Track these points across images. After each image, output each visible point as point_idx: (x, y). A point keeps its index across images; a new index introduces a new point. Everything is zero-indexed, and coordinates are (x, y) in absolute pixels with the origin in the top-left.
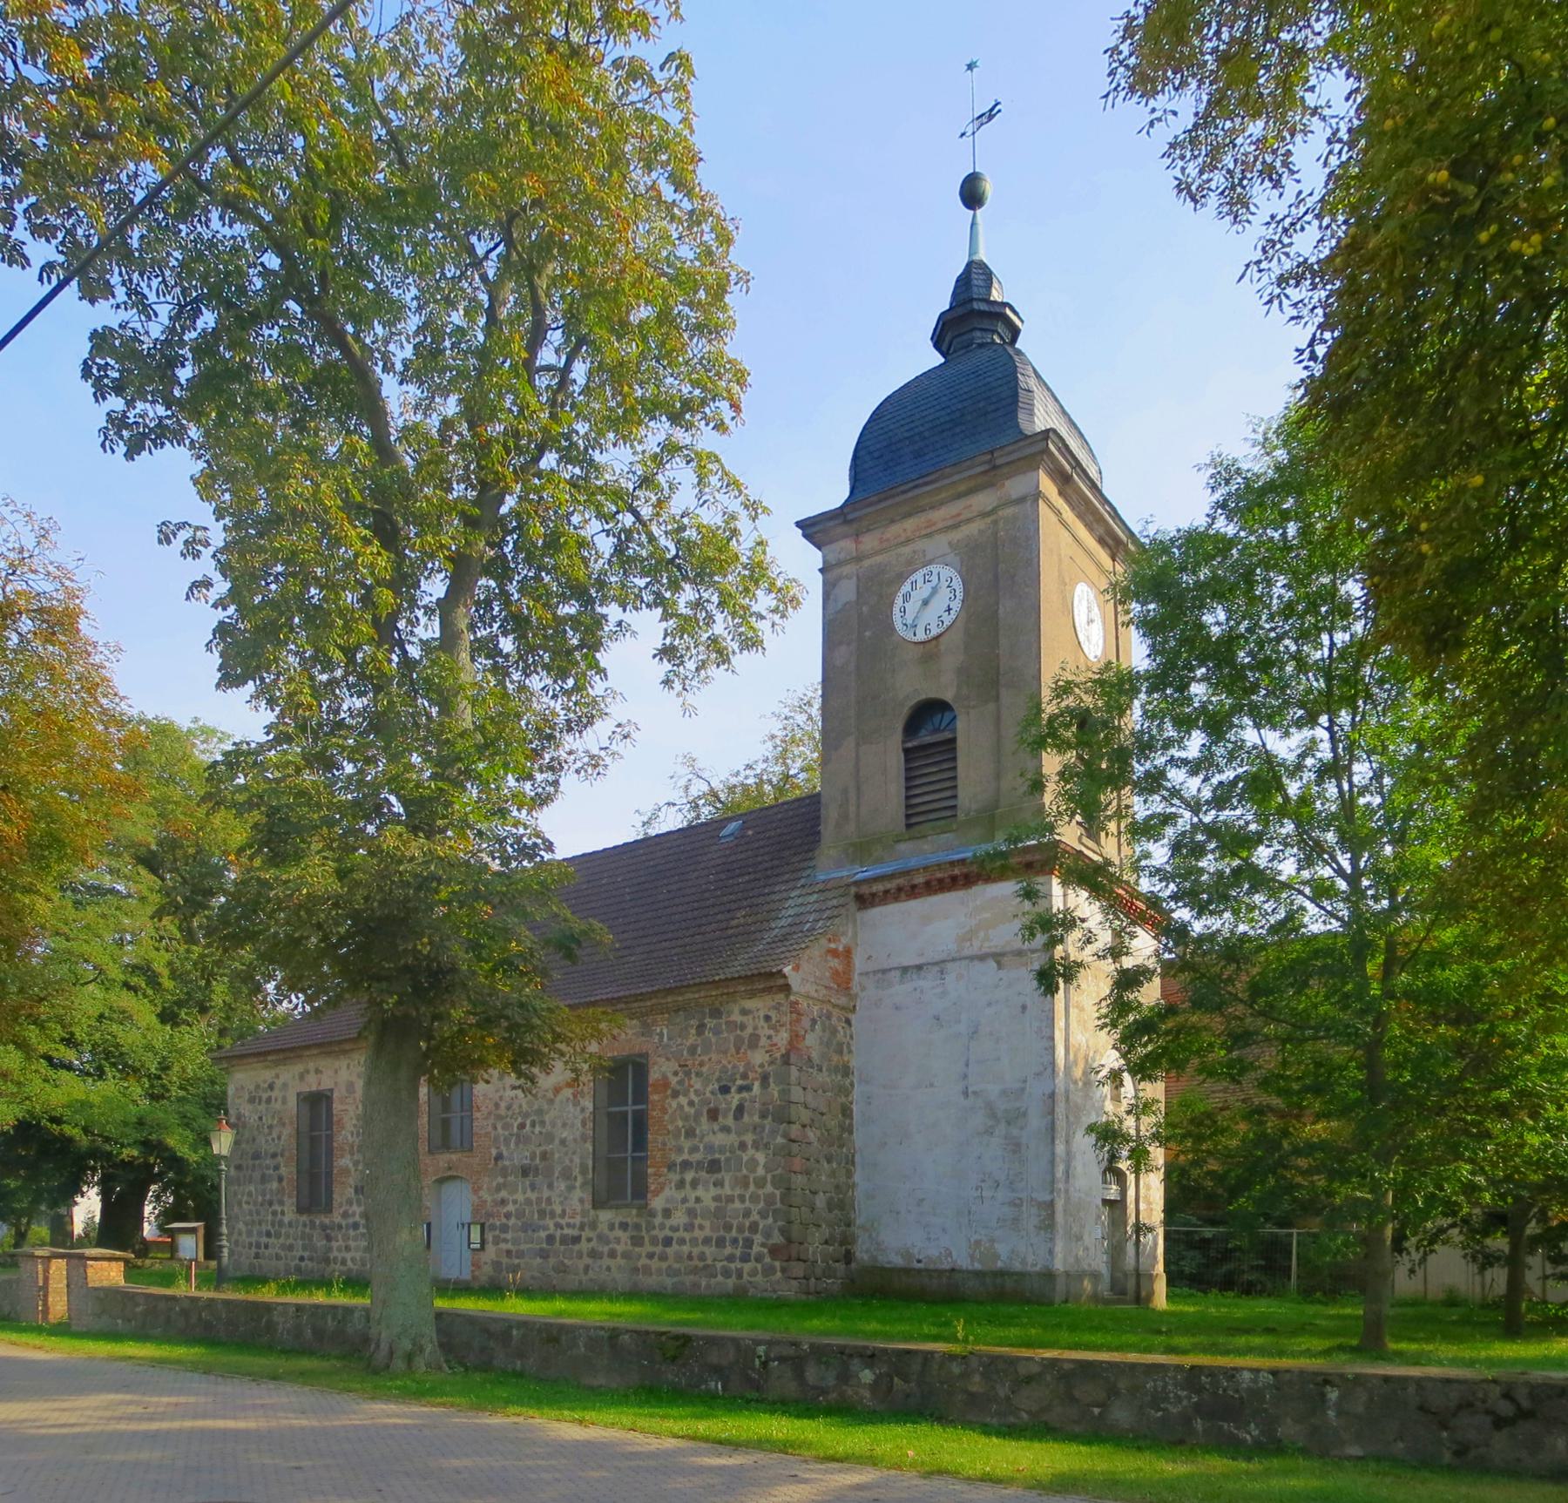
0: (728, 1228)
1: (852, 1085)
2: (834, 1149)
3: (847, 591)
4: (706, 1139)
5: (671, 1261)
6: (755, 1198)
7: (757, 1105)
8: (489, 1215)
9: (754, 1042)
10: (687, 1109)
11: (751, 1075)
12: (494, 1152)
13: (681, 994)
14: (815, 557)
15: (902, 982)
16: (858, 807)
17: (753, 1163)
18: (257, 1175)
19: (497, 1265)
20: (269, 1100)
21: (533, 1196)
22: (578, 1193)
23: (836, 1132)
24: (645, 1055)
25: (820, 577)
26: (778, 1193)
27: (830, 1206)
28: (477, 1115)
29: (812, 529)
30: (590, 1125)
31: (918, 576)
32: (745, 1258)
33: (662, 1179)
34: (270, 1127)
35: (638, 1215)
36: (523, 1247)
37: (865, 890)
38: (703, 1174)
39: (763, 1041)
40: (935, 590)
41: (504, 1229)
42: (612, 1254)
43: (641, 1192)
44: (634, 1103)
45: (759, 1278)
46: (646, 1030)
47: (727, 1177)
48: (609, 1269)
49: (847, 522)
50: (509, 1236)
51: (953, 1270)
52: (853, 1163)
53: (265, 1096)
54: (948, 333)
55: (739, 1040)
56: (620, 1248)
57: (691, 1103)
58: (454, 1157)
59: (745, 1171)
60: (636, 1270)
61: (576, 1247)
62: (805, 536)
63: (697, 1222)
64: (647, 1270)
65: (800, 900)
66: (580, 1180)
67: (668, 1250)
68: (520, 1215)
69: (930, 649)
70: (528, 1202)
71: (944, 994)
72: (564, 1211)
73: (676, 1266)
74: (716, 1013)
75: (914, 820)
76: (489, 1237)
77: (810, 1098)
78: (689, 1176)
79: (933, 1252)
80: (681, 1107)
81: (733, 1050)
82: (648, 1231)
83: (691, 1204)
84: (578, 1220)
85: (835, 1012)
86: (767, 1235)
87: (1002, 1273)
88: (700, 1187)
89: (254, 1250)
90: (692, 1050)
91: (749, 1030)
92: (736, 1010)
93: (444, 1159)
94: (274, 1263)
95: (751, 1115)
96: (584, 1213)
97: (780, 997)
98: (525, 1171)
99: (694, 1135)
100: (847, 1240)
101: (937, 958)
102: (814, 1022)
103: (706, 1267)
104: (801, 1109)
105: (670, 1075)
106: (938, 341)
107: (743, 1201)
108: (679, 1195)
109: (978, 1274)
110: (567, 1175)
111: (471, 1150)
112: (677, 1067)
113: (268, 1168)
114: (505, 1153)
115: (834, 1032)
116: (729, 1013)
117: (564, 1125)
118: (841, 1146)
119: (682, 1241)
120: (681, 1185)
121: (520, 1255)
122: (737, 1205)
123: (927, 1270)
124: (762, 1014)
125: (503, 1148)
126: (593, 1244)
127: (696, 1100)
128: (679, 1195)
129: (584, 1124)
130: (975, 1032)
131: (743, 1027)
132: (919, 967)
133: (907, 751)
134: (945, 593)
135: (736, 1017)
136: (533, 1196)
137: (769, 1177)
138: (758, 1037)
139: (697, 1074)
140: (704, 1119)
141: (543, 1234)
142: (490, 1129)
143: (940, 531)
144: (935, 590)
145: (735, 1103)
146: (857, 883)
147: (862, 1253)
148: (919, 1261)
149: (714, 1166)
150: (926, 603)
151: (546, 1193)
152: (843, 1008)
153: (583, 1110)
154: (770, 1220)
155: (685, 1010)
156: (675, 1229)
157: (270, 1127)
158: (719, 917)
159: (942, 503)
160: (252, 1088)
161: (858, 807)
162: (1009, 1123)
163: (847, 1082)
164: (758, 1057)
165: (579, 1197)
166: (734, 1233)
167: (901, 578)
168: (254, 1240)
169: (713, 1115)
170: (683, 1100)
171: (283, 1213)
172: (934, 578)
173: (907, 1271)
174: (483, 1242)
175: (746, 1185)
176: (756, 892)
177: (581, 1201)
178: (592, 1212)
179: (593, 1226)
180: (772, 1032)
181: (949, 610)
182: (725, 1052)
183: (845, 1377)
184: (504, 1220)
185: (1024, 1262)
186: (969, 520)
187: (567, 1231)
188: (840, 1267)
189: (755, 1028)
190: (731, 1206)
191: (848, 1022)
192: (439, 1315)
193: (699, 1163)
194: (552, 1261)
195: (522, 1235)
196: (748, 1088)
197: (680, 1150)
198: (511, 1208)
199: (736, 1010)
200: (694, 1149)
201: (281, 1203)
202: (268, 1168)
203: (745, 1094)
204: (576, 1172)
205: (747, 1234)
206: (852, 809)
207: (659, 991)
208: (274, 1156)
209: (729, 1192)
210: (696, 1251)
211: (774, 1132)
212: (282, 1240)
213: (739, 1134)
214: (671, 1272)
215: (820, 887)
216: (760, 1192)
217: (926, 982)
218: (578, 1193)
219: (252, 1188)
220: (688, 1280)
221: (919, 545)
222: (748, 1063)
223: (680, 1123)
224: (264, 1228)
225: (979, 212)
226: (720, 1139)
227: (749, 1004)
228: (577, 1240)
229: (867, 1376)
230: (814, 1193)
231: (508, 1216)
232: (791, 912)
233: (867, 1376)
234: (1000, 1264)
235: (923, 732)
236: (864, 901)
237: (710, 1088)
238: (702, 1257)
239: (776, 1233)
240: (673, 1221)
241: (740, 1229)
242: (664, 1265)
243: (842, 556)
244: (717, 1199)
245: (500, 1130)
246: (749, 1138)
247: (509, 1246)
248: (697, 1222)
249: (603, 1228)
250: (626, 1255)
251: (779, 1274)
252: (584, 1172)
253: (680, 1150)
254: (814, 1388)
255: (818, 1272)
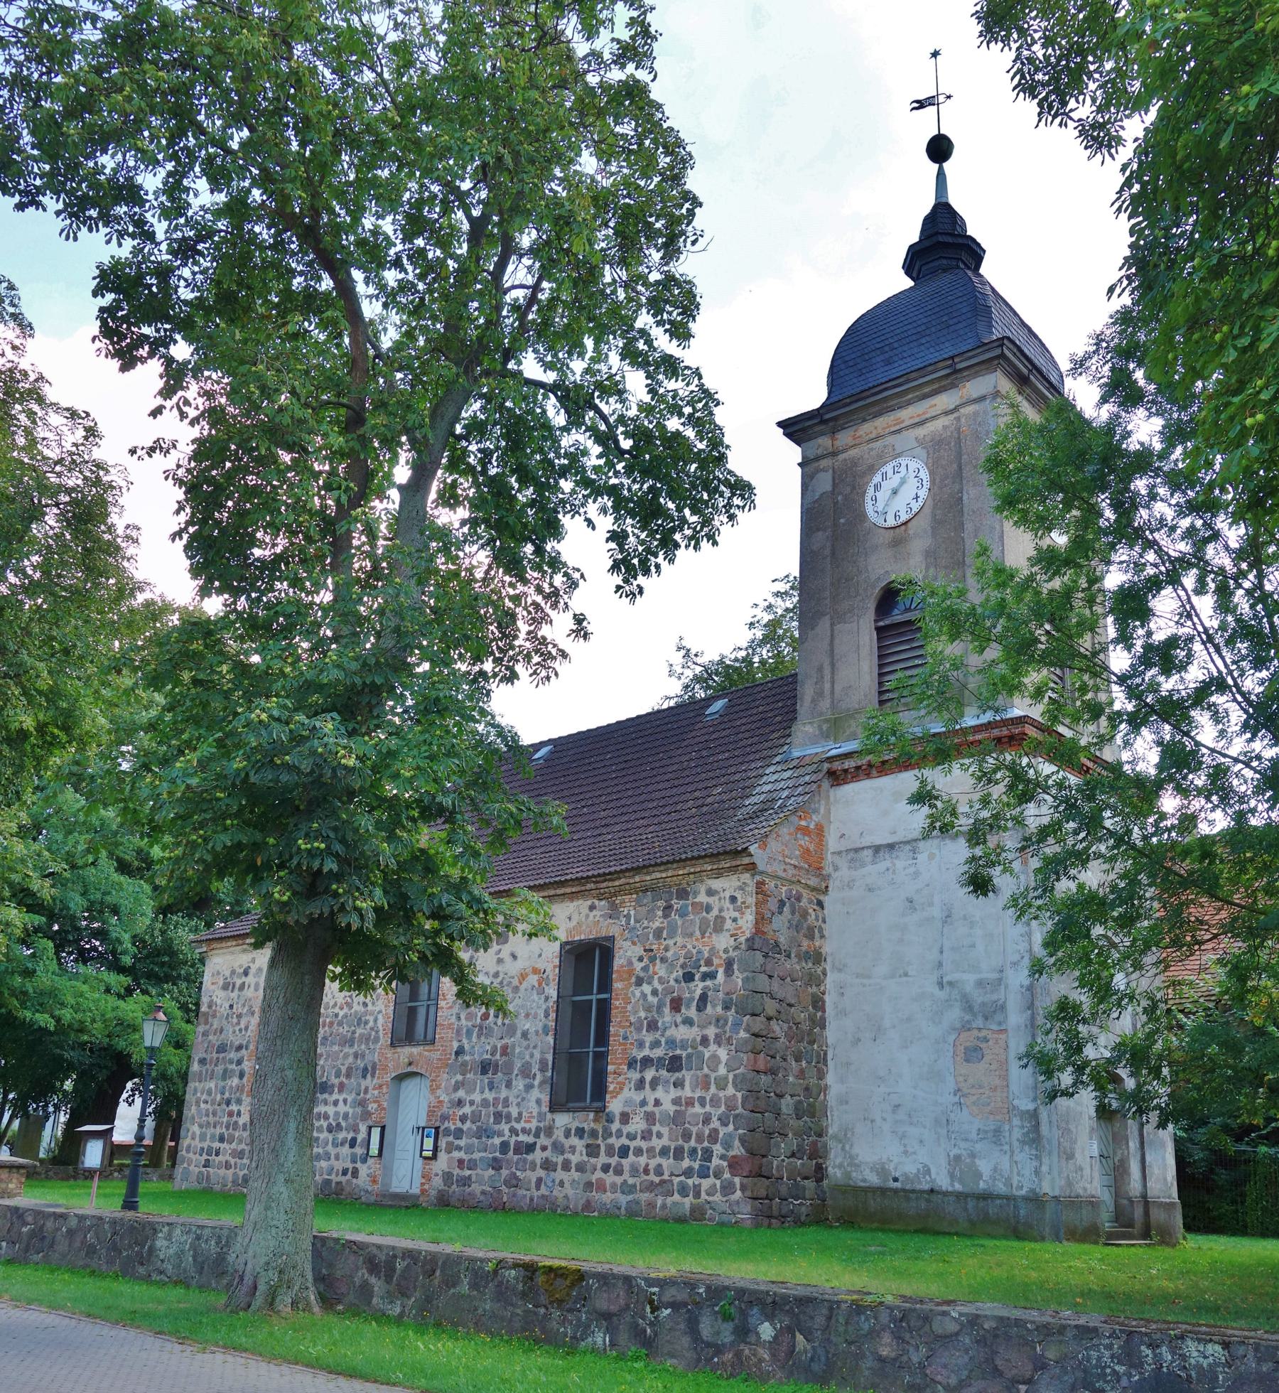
0: (687, 1136)
1: (825, 974)
2: (803, 1046)
3: (824, 483)
4: (668, 1033)
5: (626, 1176)
6: (715, 1102)
7: (721, 995)
8: (445, 1118)
9: (719, 925)
10: (650, 998)
11: (716, 961)
12: (455, 1045)
13: (648, 873)
14: (793, 453)
15: (874, 863)
16: (833, 683)
17: (714, 1057)
18: (219, 1069)
19: (447, 1177)
20: (242, 987)
21: (489, 1096)
22: (535, 1094)
23: (805, 1026)
24: (612, 939)
25: (799, 470)
26: (739, 1095)
27: (799, 1114)
28: (442, 1003)
29: (794, 428)
30: (553, 1015)
31: (888, 468)
32: (704, 1174)
33: (621, 1079)
34: (240, 1016)
35: (595, 1120)
36: (477, 1156)
37: (837, 766)
38: (664, 1073)
39: (729, 924)
40: (903, 482)
41: (459, 1133)
42: (566, 1166)
43: (600, 1091)
44: (599, 992)
45: (717, 1198)
46: (614, 912)
47: (687, 1075)
48: (562, 1184)
49: (823, 422)
50: (462, 1143)
51: (932, 1191)
52: (825, 1060)
53: (239, 982)
54: (916, 261)
55: (704, 923)
56: (575, 1159)
57: (655, 992)
58: (415, 1050)
59: (706, 1070)
60: (589, 1185)
61: (530, 1157)
62: (785, 434)
63: (655, 1129)
64: (601, 1187)
65: (775, 777)
66: (539, 1078)
67: (624, 1161)
68: (476, 1117)
69: (900, 534)
70: (485, 1103)
71: (917, 874)
72: (520, 1114)
73: (631, 1181)
74: (683, 894)
75: (886, 696)
76: (443, 1143)
77: (776, 985)
78: (649, 1074)
79: (910, 1168)
80: (644, 996)
81: (698, 933)
82: (604, 1139)
83: (649, 1108)
84: (533, 1125)
85: (805, 893)
86: (727, 1146)
87: (986, 1197)
88: (660, 1088)
89: (205, 1157)
90: (658, 933)
91: (715, 912)
92: (703, 889)
93: (406, 1052)
94: (222, 1172)
95: (714, 1006)
96: (541, 1117)
97: (746, 877)
98: (485, 1067)
99: (657, 1028)
100: (817, 1153)
101: (910, 837)
102: (782, 904)
103: (663, 1182)
104: (767, 999)
105: (634, 960)
106: (910, 266)
107: (703, 1105)
108: (638, 1097)
109: (960, 1196)
110: (526, 1072)
111: (433, 1042)
112: (642, 953)
113: (231, 1062)
114: (467, 1047)
115: (805, 914)
116: (696, 894)
117: (527, 1016)
118: (812, 1042)
119: (639, 1152)
120: (640, 1085)
121: (472, 1165)
122: (697, 1109)
123: (904, 1190)
124: (727, 894)
125: (465, 1041)
126: (548, 1153)
127: (660, 988)
128: (638, 1097)
129: (547, 1016)
130: (948, 916)
131: (708, 909)
132: (891, 847)
133: (879, 630)
134: (913, 483)
135: (702, 898)
136: (489, 1096)
137: (731, 1077)
138: (723, 919)
139: (663, 960)
140: (667, 1010)
141: (497, 1141)
142: (453, 1019)
143: (907, 428)
144: (903, 482)
145: (699, 992)
146: (831, 759)
147: (835, 1170)
148: (896, 1180)
149: (674, 1064)
150: (895, 492)
151: (504, 1093)
152: (814, 889)
153: (547, 999)
154: (731, 1127)
155: (653, 890)
156: (632, 1137)
157: (240, 1016)
158: (697, 794)
159: (909, 403)
160: (228, 973)
161: (833, 683)
162: (986, 1019)
163: (819, 971)
164: (722, 942)
165: (540, 1095)
166: (693, 1143)
167: (872, 470)
168: (205, 1145)
169: (676, 1005)
170: (647, 988)
171: (239, 1114)
172: (903, 469)
173: (882, 1191)
174: (436, 1149)
175: (706, 1087)
176: (733, 770)
177: (538, 1102)
178: (549, 1116)
179: (549, 1131)
180: (736, 914)
181: (917, 497)
182: (691, 935)
183: (744, 1332)
184: (459, 1124)
185: (1008, 1183)
186: (934, 418)
187: (522, 1138)
188: (810, 1184)
189: (721, 910)
190: (691, 1111)
191: (820, 904)
192: (320, 1243)
193: (660, 1059)
194: (505, 1172)
195: (476, 1141)
196: (711, 976)
197: (641, 1045)
198: (467, 1110)
199: (703, 889)
200: (656, 1044)
201: (239, 1102)
202: (231, 1062)
203: (709, 983)
204: (535, 1069)
205: (706, 1144)
206: (827, 686)
207: (627, 870)
208: (239, 1048)
209: (689, 1094)
210: (653, 1163)
211: (737, 1025)
212: (234, 1145)
213: (701, 1027)
214: (627, 1189)
215: (794, 763)
216: (721, 1094)
217: (901, 862)
218: (535, 1094)
219: (212, 1085)
220: (644, 1197)
221: (890, 440)
222: (712, 949)
223: (642, 1014)
224: (218, 1131)
225: (945, 165)
226: (682, 1033)
227: (716, 884)
228: (530, 1148)
229: (766, 1331)
230: (781, 1096)
231: (463, 1119)
232: (767, 788)
233: (766, 1331)
234: (982, 1185)
235: (896, 611)
236: (837, 778)
237: (674, 975)
238: (659, 1171)
239: (737, 1143)
240: (627, 1129)
241: (700, 1139)
242: (619, 1180)
243: (819, 452)
244: (676, 1102)
245: (463, 1022)
246: (711, 1032)
247: (461, 1155)
248: (655, 1129)
249: (559, 1134)
250: (581, 1168)
251: (739, 1193)
252: (543, 1069)
253: (641, 1045)
254: (709, 1345)
255: (784, 1190)
